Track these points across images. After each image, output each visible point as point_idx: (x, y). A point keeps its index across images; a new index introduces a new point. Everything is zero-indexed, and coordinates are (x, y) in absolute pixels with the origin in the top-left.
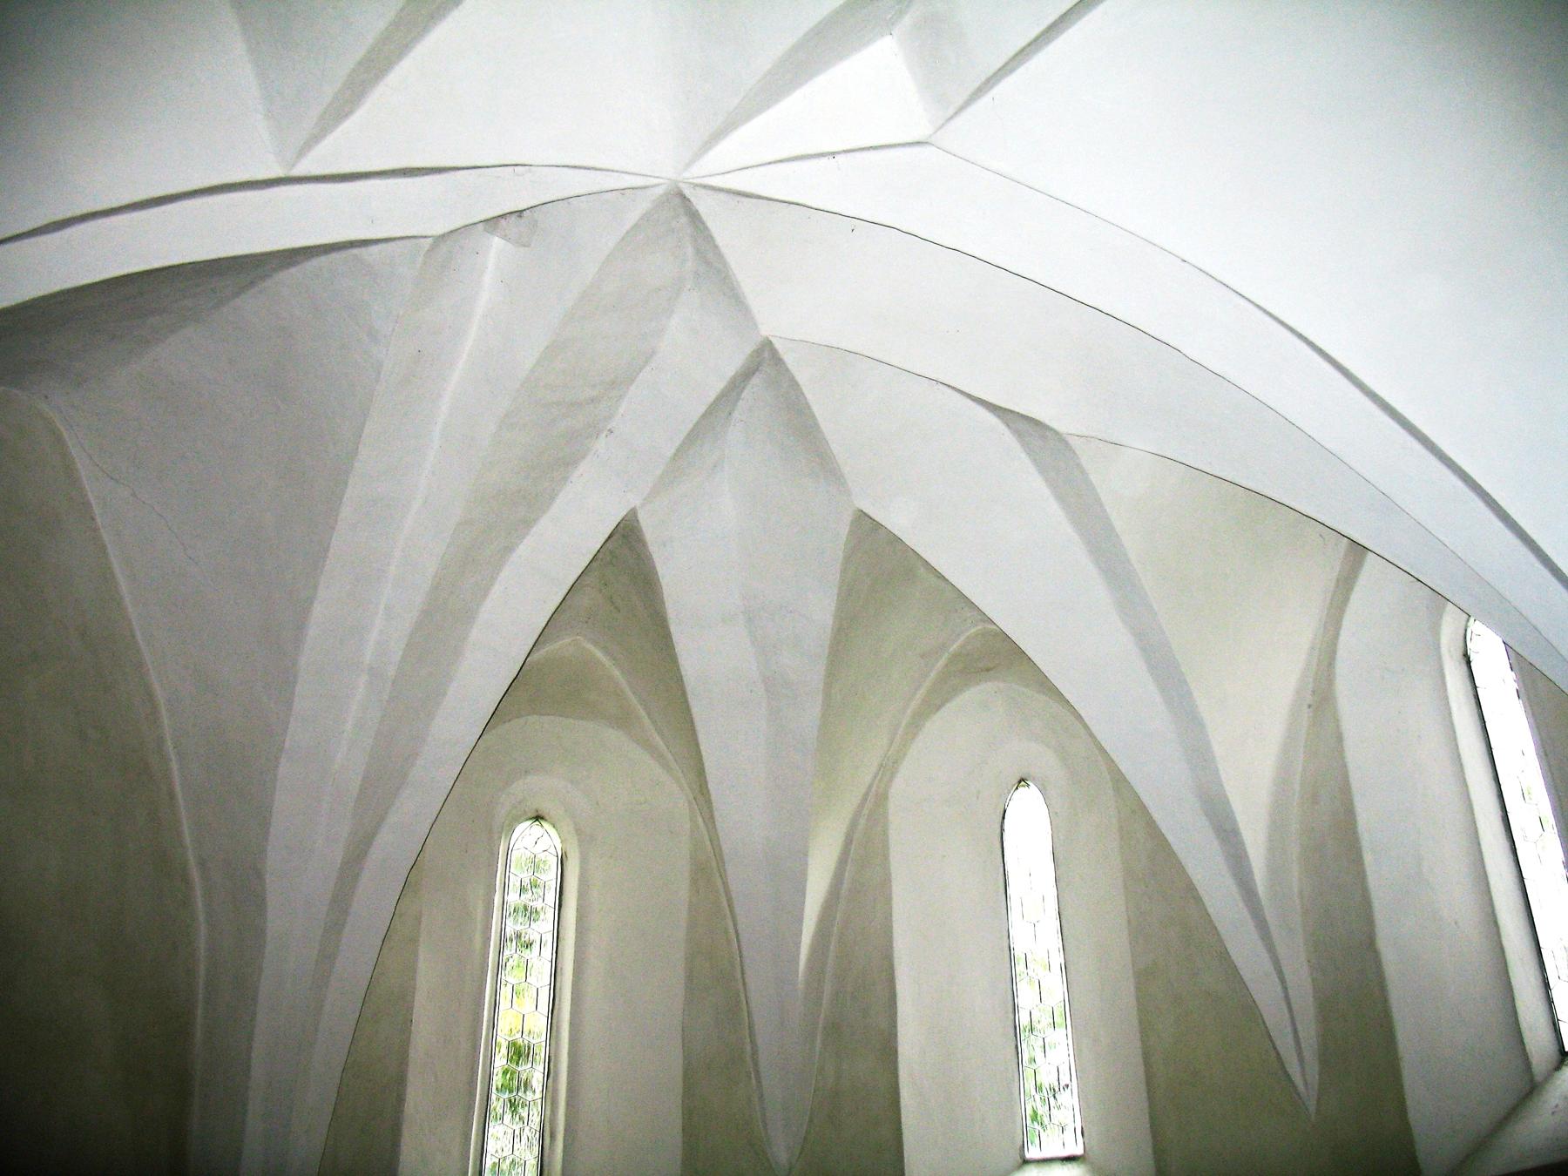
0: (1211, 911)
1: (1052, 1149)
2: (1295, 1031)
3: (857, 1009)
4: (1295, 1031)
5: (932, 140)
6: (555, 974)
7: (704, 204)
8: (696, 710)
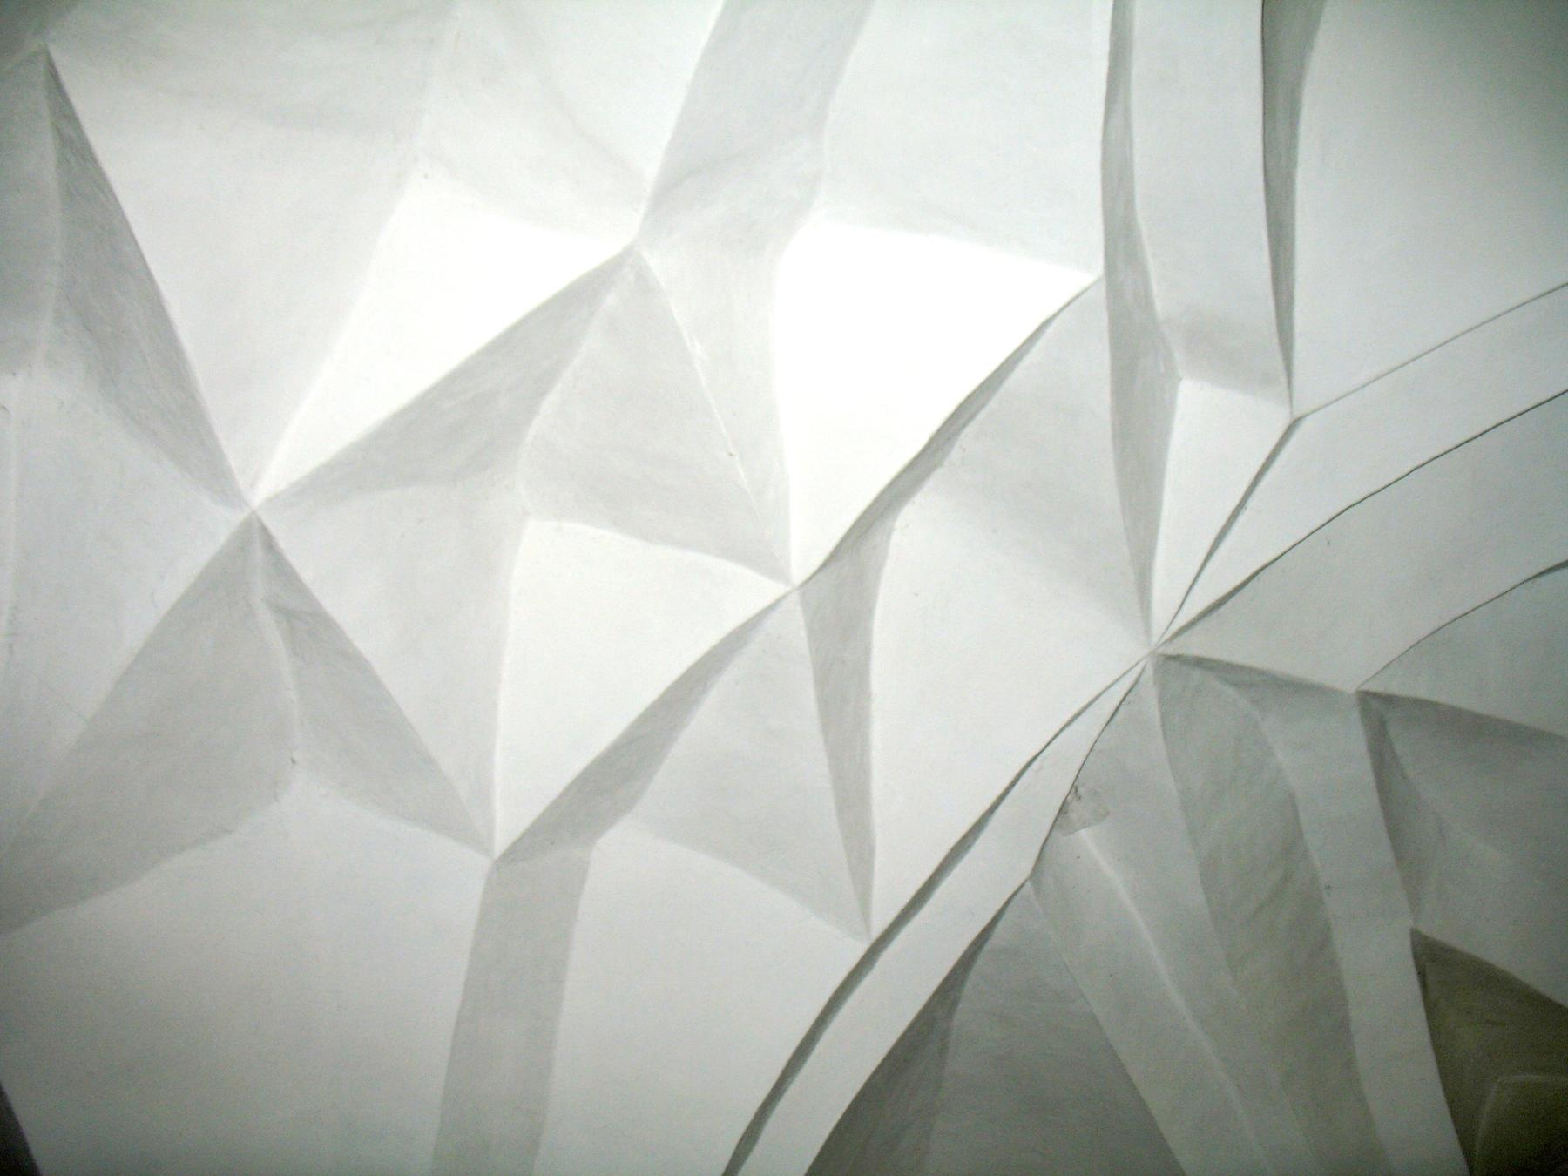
5: (1297, 414)
7: (1195, 645)
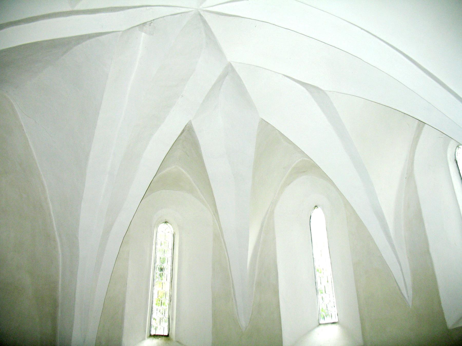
0: (377, 244)
1: (328, 320)
2: (404, 280)
3: (266, 281)
4: (404, 280)
6: (172, 270)
7: (207, 17)
8: (213, 185)
